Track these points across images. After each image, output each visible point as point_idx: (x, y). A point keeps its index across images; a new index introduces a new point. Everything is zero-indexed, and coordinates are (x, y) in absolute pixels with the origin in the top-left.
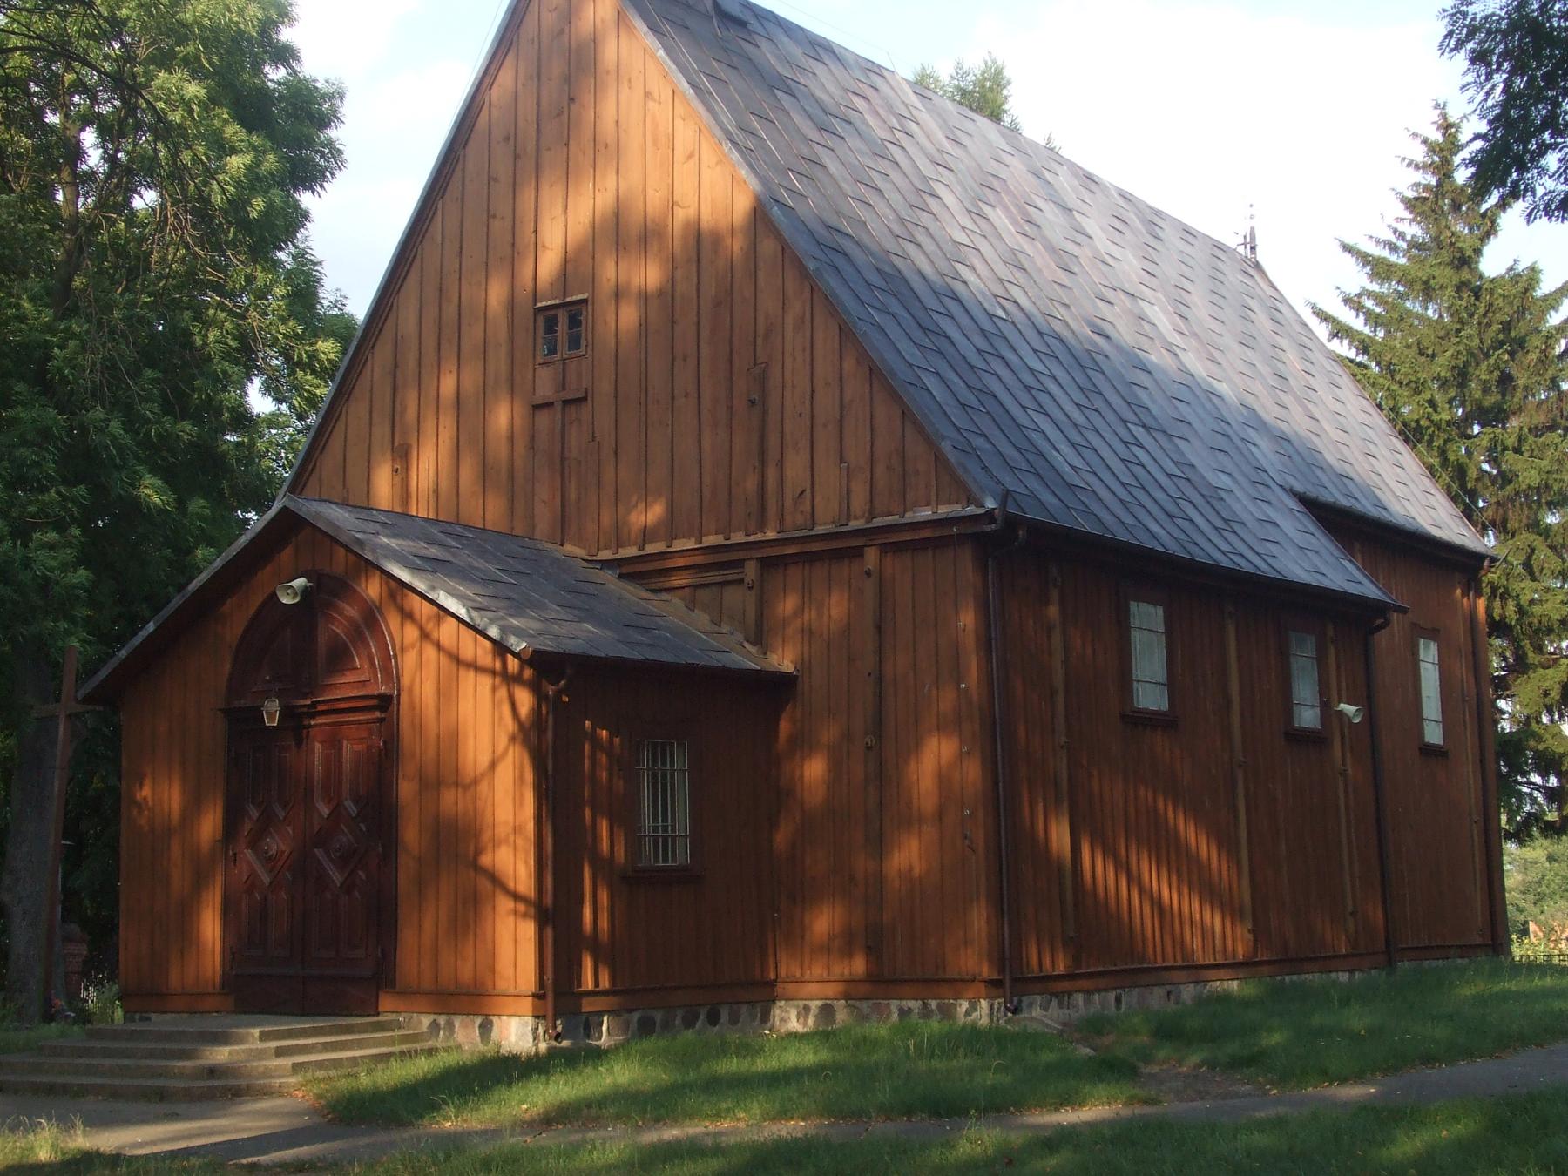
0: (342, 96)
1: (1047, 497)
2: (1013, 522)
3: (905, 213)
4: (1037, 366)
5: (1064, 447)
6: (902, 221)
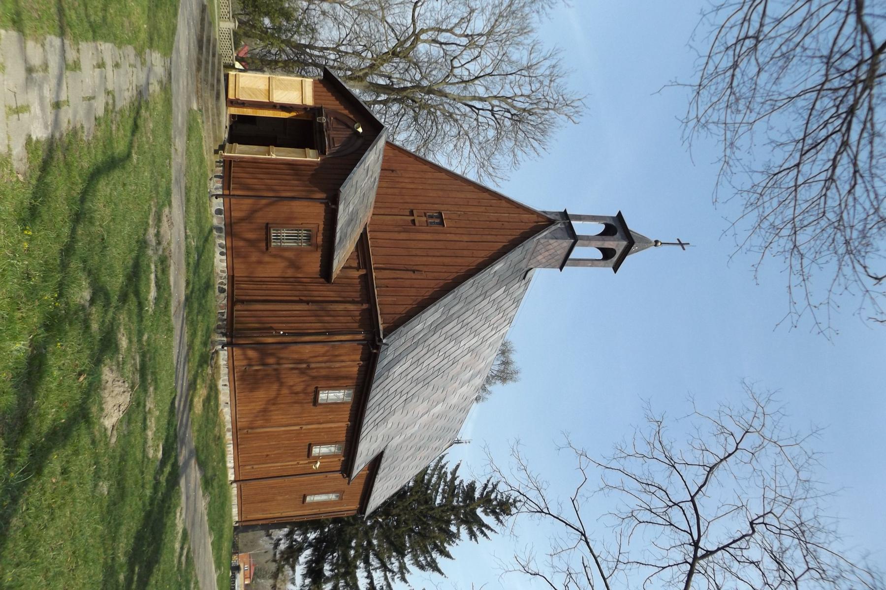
0: (515, 381)
1: (385, 362)
2: (378, 348)
5: (401, 370)
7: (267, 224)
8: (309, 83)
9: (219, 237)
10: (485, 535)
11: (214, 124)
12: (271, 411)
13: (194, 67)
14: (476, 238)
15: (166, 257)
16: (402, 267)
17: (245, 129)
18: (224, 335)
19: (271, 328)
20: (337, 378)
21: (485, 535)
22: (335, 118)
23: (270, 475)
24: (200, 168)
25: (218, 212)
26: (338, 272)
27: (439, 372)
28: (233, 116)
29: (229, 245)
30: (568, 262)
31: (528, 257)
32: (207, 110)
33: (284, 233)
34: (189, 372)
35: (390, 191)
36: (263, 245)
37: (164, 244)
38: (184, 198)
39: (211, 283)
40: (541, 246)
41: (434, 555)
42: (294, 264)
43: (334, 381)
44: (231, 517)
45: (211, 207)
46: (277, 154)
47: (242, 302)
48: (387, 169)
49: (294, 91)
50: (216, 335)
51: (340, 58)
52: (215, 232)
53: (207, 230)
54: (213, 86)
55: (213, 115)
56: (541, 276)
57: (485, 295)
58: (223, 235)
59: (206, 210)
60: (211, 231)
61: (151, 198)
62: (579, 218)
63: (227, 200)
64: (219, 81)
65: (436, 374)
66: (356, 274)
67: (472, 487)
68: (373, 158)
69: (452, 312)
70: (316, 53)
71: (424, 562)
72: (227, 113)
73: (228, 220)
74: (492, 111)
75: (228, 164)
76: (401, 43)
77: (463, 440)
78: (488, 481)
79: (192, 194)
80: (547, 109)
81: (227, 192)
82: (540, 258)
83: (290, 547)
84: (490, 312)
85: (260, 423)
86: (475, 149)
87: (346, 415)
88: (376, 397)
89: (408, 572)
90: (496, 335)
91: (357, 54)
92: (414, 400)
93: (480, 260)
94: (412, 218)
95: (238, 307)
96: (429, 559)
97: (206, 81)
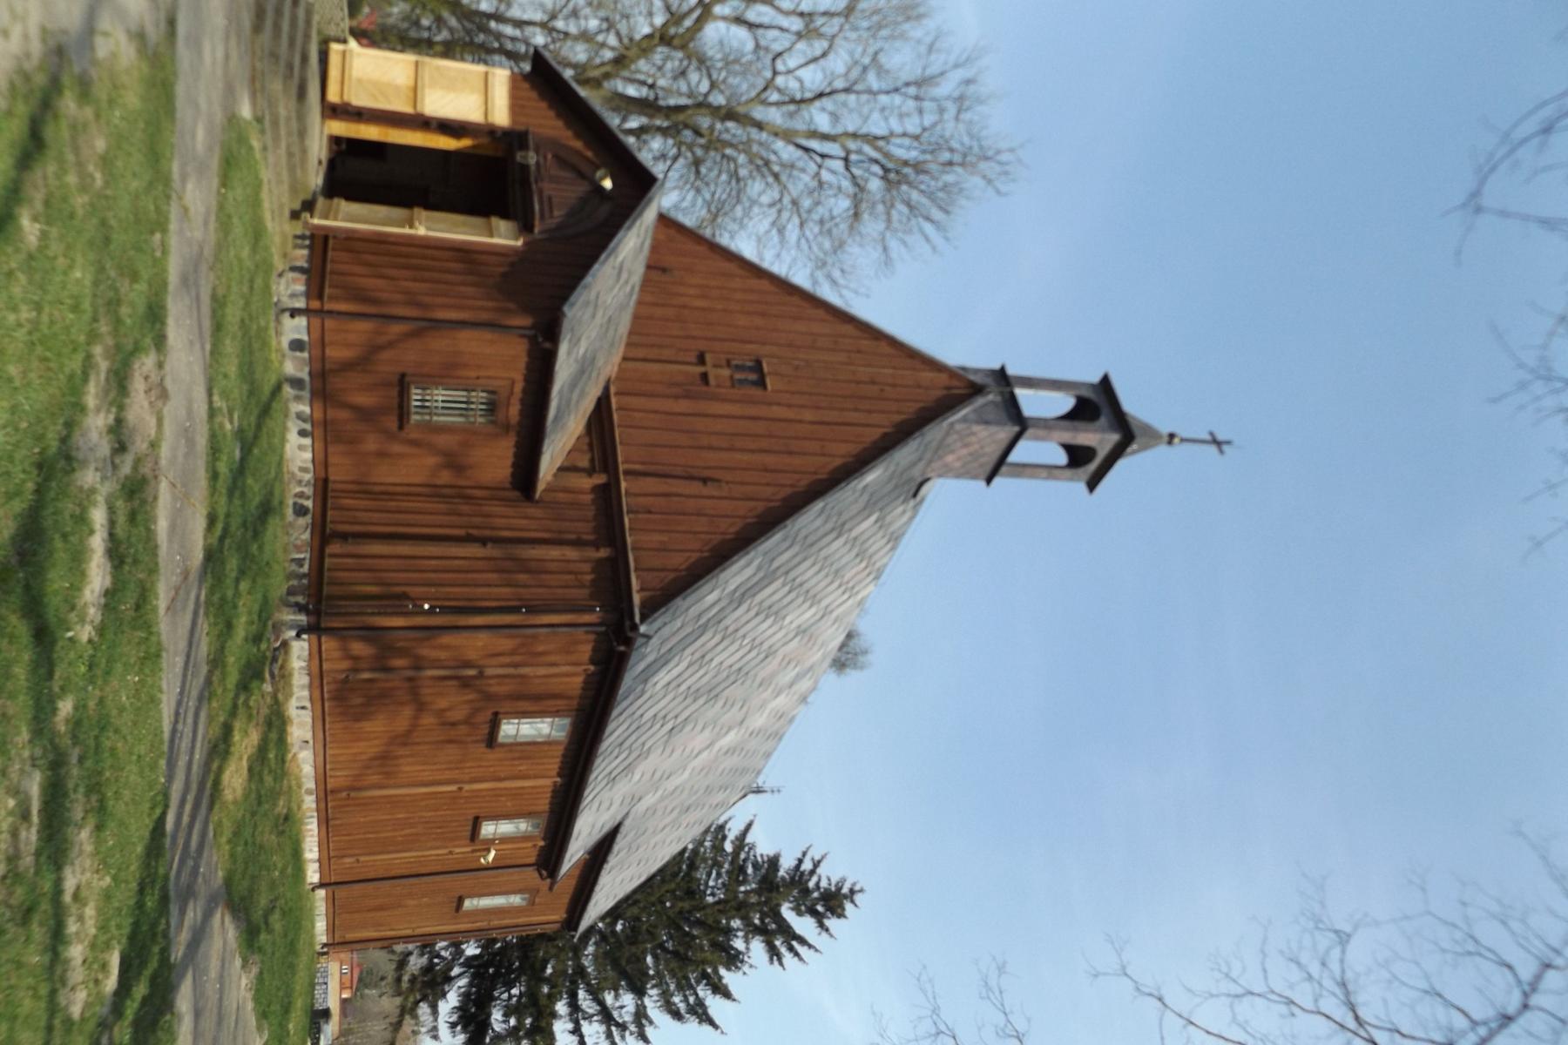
0: (862, 668)
1: (642, 666)
2: (629, 642)
3: (806, 587)
4: (714, 664)
6: (801, 585)
7: (403, 376)
8: (501, 77)
9: (298, 398)
10: (797, 954)
11: (290, 155)
12: (396, 758)
13: (247, 21)
14: (833, 416)
15: (143, 481)
16: (679, 471)
17: (361, 169)
18: (301, 608)
19: (405, 596)
20: (538, 698)
21: (797, 954)
22: (556, 156)
23: (393, 873)
24: (254, 249)
25: (297, 345)
26: (549, 478)
27: (739, 674)
28: (336, 140)
29: (318, 415)
30: (1004, 469)
31: (928, 455)
32: (275, 123)
33: (440, 395)
34: (211, 719)
35: (659, 312)
36: (391, 422)
37: (140, 446)
38: (207, 323)
39: (275, 502)
40: (955, 437)
41: (701, 994)
42: (454, 462)
43: (533, 703)
44: (313, 936)
45: (278, 333)
46: (427, 227)
47: (344, 537)
48: (655, 266)
49: (471, 94)
50: (286, 610)
51: (554, 41)
52: (288, 390)
53: (267, 390)
54: (290, 67)
55: (289, 134)
56: (950, 496)
57: (840, 530)
58: (306, 394)
59: (265, 344)
60: (277, 389)
61: (93, 337)
62: (1029, 383)
63: (316, 322)
64: (305, 59)
65: (732, 678)
66: (586, 482)
67: (774, 862)
68: (632, 245)
69: (776, 564)
70: (508, 30)
71: (682, 1007)
72: (320, 134)
73: (318, 366)
74: (846, 160)
75: (320, 243)
76: (675, 18)
77: (767, 786)
78: (804, 854)
79: (229, 310)
80: (950, 163)
81: (315, 304)
82: (950, 458)
83: (429, 969)
84: (844, 561)
85: (375, 779)
86: (808, 233)
87: (553, 764)
88: (617, 730)
89: (651, 1022)
90: (850, 602)
91: (585, 36)
92: (688, 728)
93: (838, 462)
94: (701, 369)
95: (334, 548)
96: (692, 1000)
97: (274, 56)
